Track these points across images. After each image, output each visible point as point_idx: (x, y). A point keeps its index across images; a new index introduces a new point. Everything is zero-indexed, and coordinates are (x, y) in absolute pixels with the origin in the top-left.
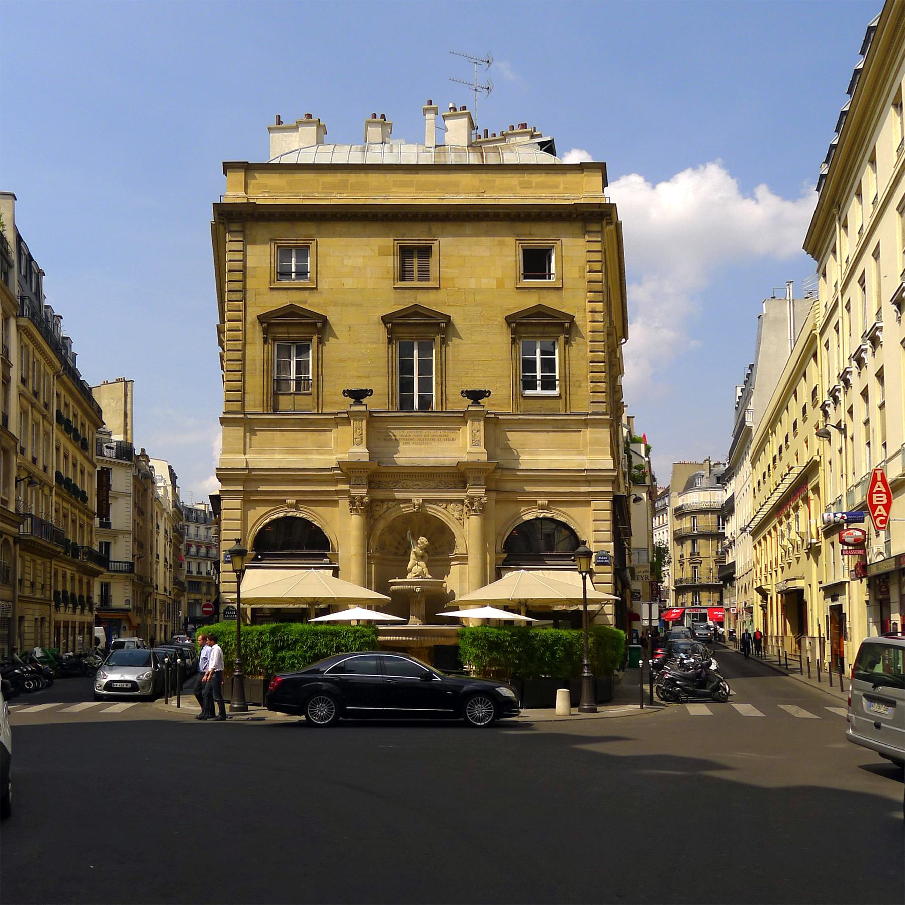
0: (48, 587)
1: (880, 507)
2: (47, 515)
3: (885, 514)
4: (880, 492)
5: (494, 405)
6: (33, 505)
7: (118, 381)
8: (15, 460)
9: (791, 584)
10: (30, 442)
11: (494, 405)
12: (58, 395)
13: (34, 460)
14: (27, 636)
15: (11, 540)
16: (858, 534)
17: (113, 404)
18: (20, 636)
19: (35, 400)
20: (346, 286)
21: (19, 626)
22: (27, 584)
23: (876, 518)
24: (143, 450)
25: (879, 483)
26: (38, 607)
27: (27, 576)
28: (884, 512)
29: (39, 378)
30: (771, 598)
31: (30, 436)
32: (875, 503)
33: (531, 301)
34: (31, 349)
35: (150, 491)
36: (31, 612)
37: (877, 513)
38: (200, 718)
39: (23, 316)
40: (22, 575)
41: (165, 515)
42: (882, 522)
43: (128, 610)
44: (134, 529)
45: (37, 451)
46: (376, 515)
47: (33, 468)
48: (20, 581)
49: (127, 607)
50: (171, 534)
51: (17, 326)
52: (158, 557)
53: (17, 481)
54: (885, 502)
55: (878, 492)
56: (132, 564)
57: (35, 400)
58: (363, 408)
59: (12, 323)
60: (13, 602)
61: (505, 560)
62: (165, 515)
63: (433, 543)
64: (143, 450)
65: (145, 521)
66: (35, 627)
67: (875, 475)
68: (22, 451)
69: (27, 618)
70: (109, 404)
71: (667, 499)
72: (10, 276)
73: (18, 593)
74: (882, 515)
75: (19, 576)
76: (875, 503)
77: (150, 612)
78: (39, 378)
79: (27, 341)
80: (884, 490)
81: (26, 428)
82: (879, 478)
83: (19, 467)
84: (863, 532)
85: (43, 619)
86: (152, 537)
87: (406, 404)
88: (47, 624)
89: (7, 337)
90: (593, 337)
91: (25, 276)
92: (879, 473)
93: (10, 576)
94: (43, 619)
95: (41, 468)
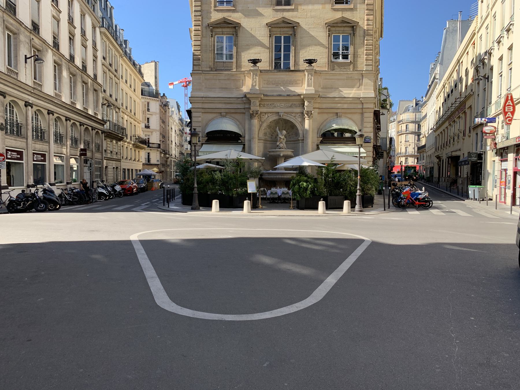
0: (119, 154)
1: (509, 113)
2: (118, 121)
3: (511, 116)
4: (510, 105)
5: (319, 67)
6: (111, 116)
7: (152, 62)
8: (101, 95)
9: (454, 154)
10: (108, 87)
11: (319, 67)
12: (122, 65)
13: (111, 96)
14: (109, 175)
15: (100, 132)
16: (493, 128)
17: (150, 72)
18: (106, 175)
19: (110, 68)
20: (250, 9)
21: (106, 170)
22: (109, 152)
23: (506, 118)
24: (164, 94)
25: (510, 101)
26: (114, 162)
27: (108, 148)
28: (511, 116)
29: (112, 57)
30: (443, 160)
31: (108, 84)
32: (506, 111)
33: (338, 15)
34: (107, 43)
35: (167, 112)
36: (111, 164)
37: (507, 116)
38: (250, 199)
39: (103, 27)
40: (106, 148)
41: (175, 123)
42: (509, 120)
43: (158, 165)
44: (160, 129)
45: (112, 92)
46: (263, 120)
47: (110, 99)
48: (105, 151)
49: (158, 163)
50: (178, 132)
51: (100, 32)
52: (172, 142)
53: (102, 105)
54: (512, 110)
55: (508, 105)
56: (159, 145)
57: (110, 68)
58: (256, 68)
59: (98, 30)
60: (102, 159)
61: (321, 141)
62: (175, 123)
63: (289, 133)
64: (164, 94)
65: (165, 126)
66: (113, 171)
67: (508, 97)
68: (105, 91)
69: (109, 167)
70: (148, 73)
71: (395, 116)
72: (96, 7)
73: (104, 156)
74: (509, 117)
75: (104, 148)
76: (506, 111)
77: (169, 166)
78: (112, 57)
79: (104, 37)
80: (512, 104)
81: (106, 81)
82: (509, 98)
83: (103, 98)
84: (495, 128)
85: (117, 168)
86: (169, 133)
87: (277, 66)
88: (119, 170)
89: (95, 37)
90: (367, 28)
91: (104, 9)
92: (510, 96)
93: (100, 148)
94: (117, 168)
95: (114, 99)
